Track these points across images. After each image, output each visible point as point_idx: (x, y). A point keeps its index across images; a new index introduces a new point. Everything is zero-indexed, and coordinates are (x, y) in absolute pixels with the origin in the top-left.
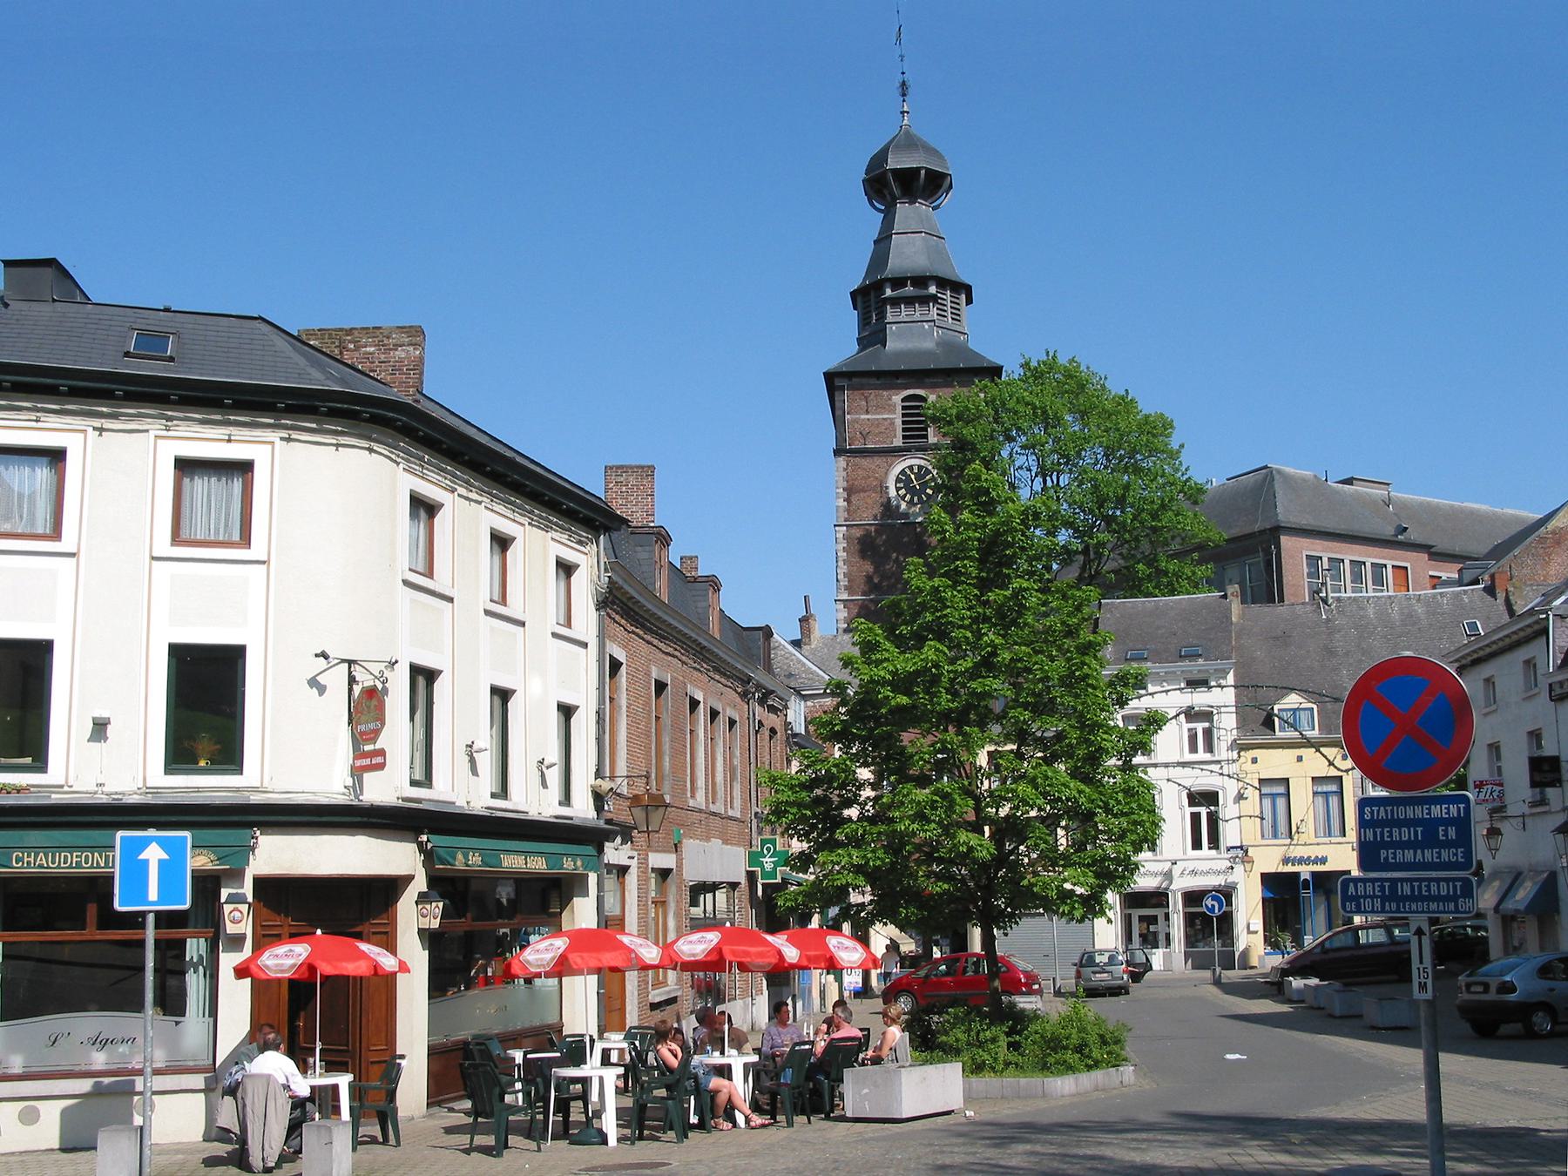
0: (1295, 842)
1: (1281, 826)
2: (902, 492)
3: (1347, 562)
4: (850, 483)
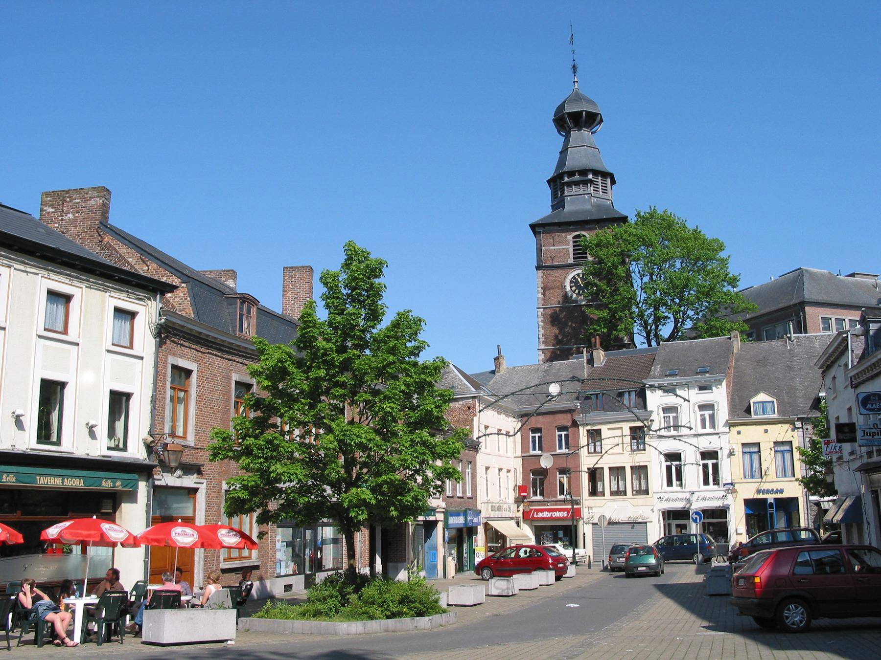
0: (764, 480)
1: (755, 471)
2: (574, 288)
3: (847, 321)
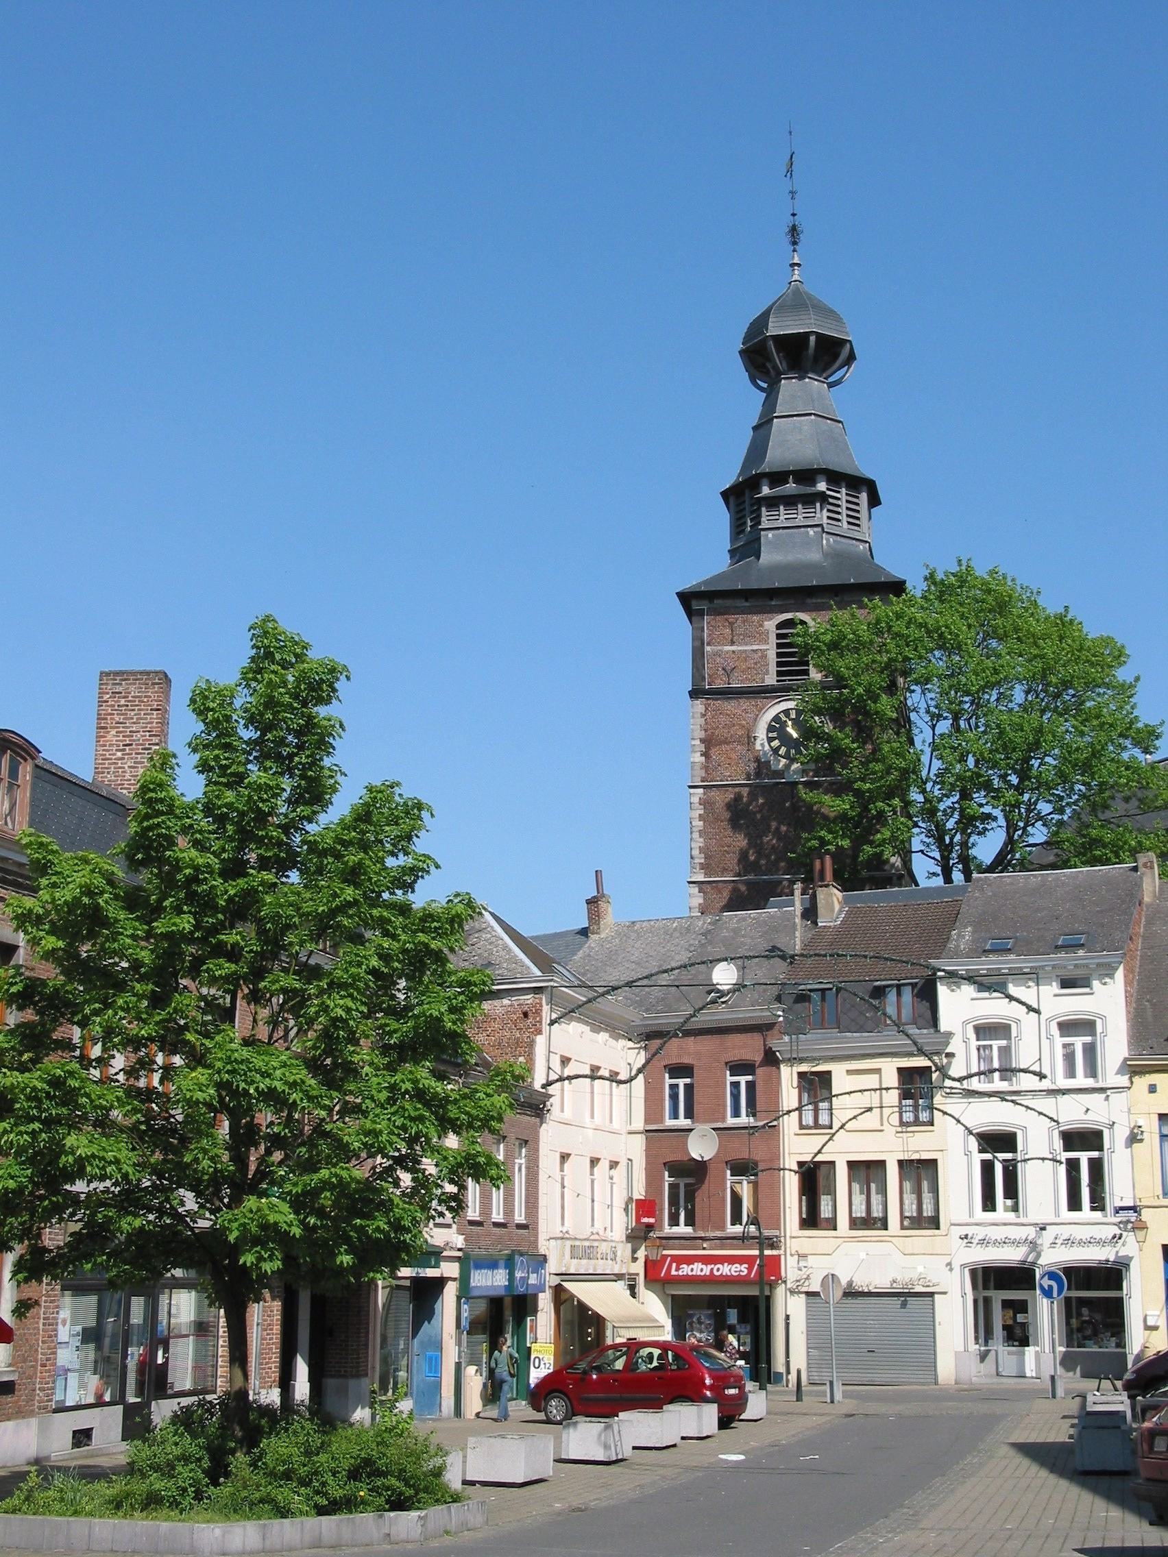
2: (776, 743)
4: (709, 732)
